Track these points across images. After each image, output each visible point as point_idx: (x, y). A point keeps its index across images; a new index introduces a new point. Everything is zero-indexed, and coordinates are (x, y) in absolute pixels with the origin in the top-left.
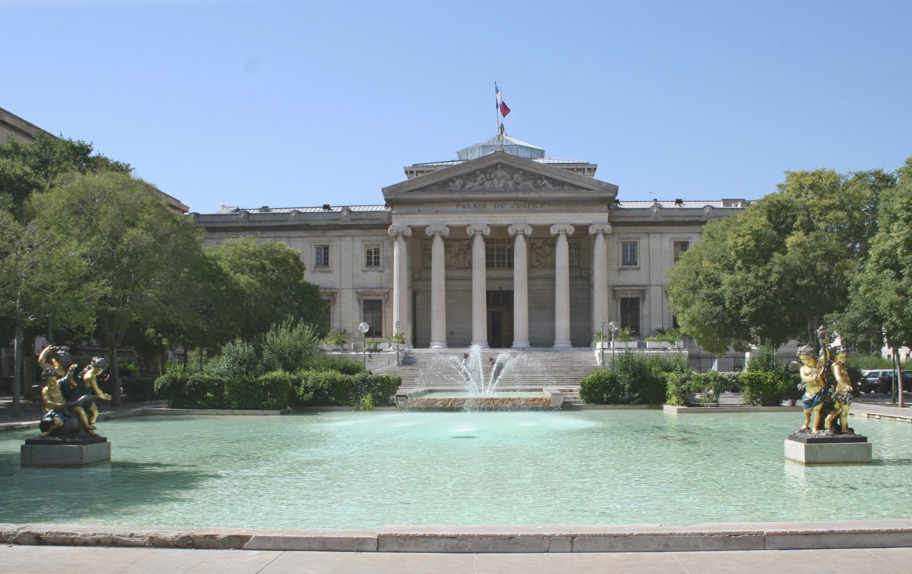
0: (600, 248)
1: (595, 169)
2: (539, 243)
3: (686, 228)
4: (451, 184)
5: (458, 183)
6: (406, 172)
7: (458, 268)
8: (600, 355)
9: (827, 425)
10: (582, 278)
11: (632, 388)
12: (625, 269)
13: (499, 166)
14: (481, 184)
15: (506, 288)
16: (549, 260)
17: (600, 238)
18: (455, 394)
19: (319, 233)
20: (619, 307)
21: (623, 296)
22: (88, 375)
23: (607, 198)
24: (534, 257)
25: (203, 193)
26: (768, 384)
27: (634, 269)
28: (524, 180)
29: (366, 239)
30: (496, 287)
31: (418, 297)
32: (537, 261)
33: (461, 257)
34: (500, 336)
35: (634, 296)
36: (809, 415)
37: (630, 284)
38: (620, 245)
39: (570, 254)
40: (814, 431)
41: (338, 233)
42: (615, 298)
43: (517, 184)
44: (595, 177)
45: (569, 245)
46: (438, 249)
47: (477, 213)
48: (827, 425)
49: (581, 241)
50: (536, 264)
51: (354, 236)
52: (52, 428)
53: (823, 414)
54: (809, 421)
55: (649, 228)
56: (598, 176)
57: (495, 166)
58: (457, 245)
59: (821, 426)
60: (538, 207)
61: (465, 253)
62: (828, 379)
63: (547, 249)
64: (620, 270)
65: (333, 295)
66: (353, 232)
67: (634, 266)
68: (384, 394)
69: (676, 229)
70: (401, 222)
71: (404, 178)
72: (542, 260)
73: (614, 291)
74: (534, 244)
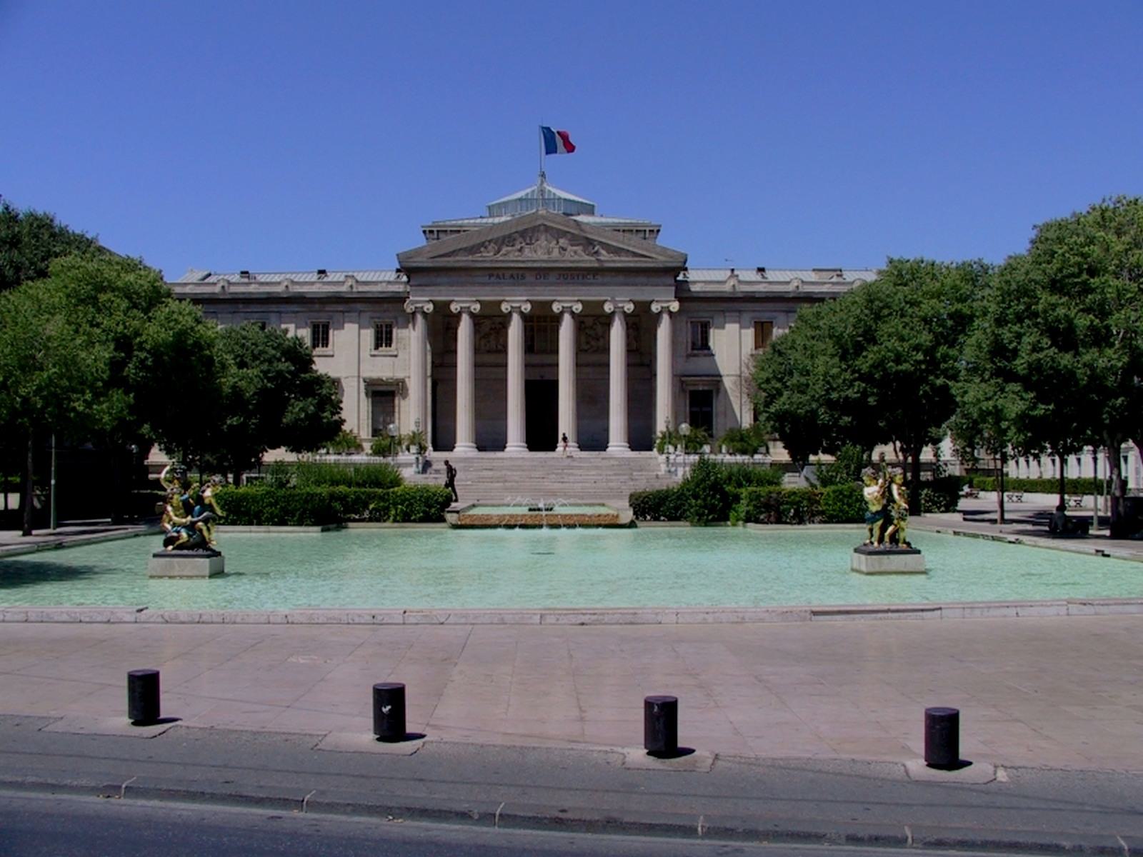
0: (663, 333)
1: (658, 231)
2: (589, 321)
3: (770, 306)
4: (482, 249)
5: (491, 246)
6: (424, 232)
7: (489, 352)
8: (669, 468)
9: (887, 539)
10: (642, 365)
11: (706, 503)
12: (695, 355)
13: (542, 228)
14: (520, 250)
15: (548, 377)
16: (601, 343)
17: (665, 318)
18: (501, 508)
19: (317, 306)
20: (688, 402)
21: (692, 388)
22: (208, 493)
23: (671, 273)
24: (583, 339)
25: (185, 269)
26: (907, 489)
27: (705, 355)
28: (572, 245)
29: (375, 315)
30: (536, 376)
31: (439, 388)
32: (588, 343)
33: (492, 337)
34: (541, 434)
35: (706, 388)
36: (871, 530)
37: (701, 373)
38: (689, 324)
39: (628, 336)
40: (876, 544)
41: (340, 308)
42: (683, 390)
43: (565, 250)
44: (658, 242)
45: (627, 324)
46: (617, 335)
47: (514, 285)
48: (887, 539)
49: (641, 327)
50: (586, 347)
51: (361, 311)
52: (178, 543)
53: (883, 529)
54: (872, 536)
55: (725, 305)
56: (661, 241)
57: (535, 229)
58: (487, 322)
59: (881, 540)
60: (590, 279)
61: (498, 333)
62: (887, 494)
63: (599, 329)
64: (688, 356)
65: (336, 383)
66: (359, 306)
67: (706, 352)
68: (432, 508)
69: (757, 306)
70: (422, 300)
71: (421, 241)
72: (593, 343)
73: (682, 382)
74: (583, 322)
